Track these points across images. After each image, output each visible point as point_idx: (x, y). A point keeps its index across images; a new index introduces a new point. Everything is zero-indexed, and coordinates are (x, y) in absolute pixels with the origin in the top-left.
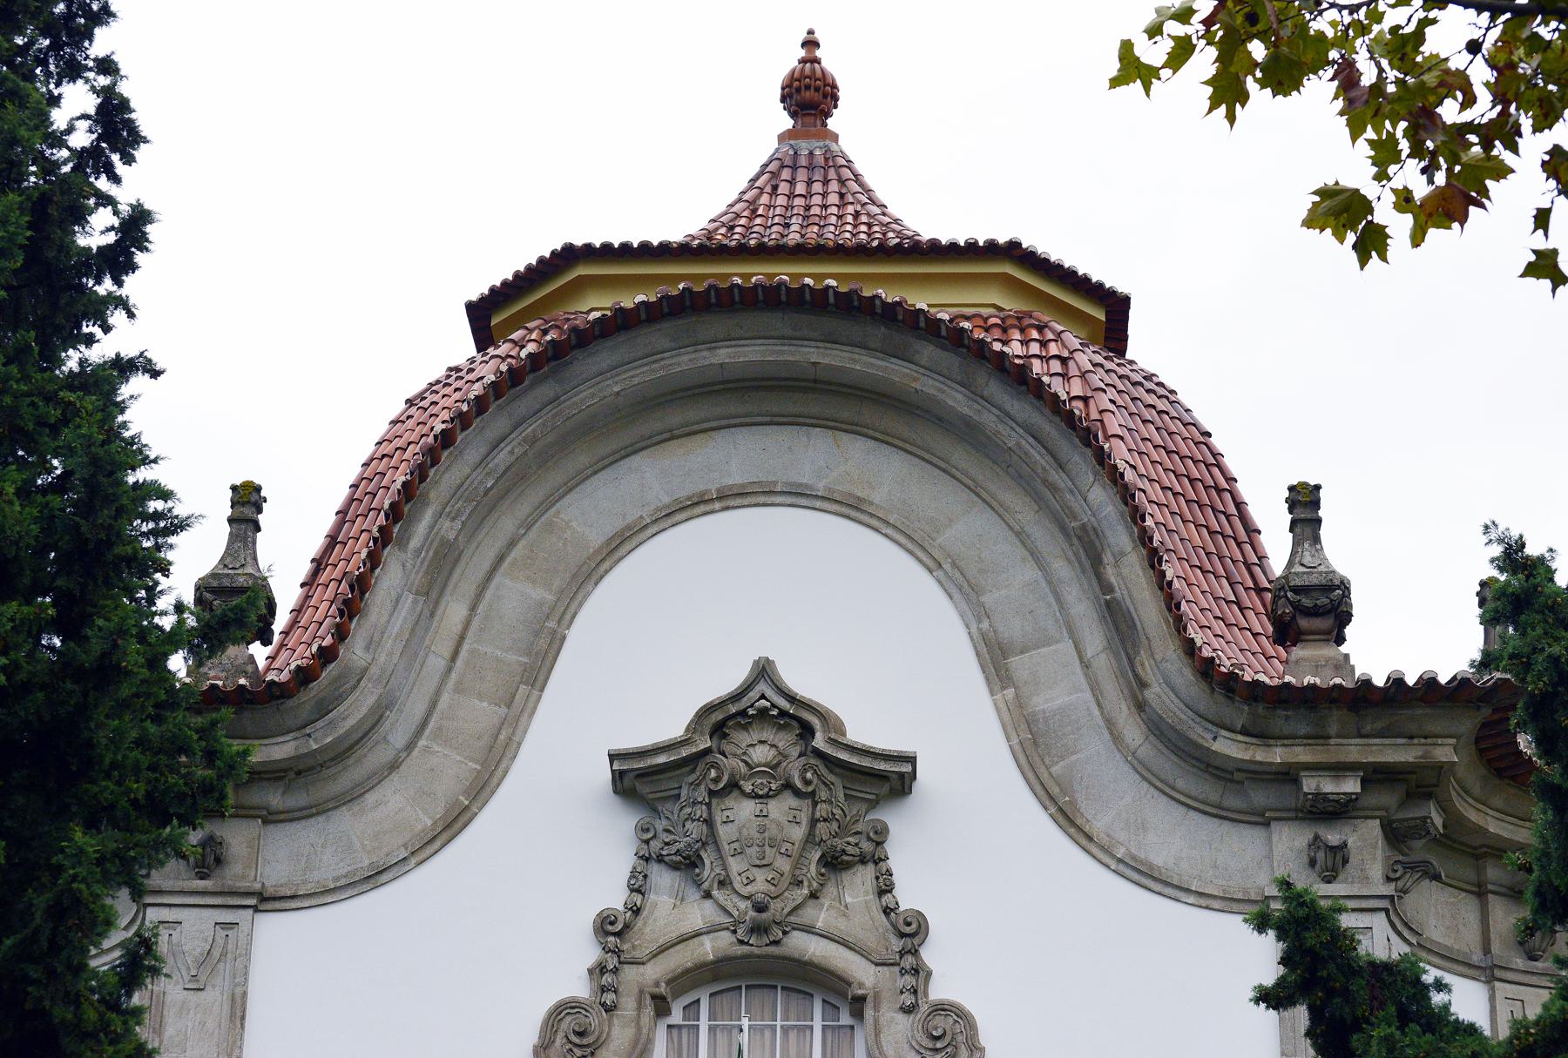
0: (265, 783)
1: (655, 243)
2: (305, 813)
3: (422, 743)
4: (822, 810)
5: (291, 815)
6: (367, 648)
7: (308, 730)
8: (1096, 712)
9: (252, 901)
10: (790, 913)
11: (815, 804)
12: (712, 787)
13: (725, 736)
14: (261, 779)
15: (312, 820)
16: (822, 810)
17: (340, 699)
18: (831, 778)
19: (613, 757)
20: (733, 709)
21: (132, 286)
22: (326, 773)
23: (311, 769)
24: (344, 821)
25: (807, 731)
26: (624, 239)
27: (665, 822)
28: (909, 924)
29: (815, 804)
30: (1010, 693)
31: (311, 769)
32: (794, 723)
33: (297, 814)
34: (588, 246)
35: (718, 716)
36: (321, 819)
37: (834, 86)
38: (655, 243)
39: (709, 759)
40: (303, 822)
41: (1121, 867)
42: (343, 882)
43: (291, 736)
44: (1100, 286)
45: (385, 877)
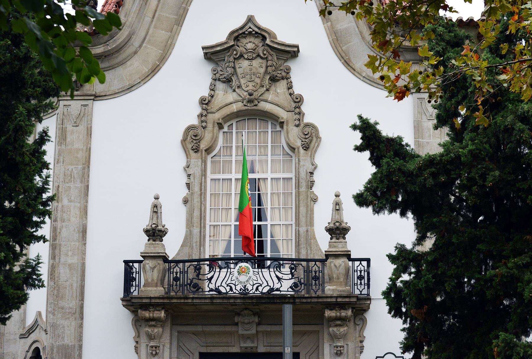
4: (270, 63)
6: (125, 16)
8: (357, 29)
11: (267, 61)
12: (235, 57)
13: (239, 40)
16: (270, 63)
18: (272, 53)
19: (203, 48)
20: (241, 32)
25: (264, 38)
27: (220, 68)
28: (297, 99)
29: (267, 61)
30: (329, 23)
32: (260, 36)
35: (236, 34)
39: (234, 48)
41: (364, 79)
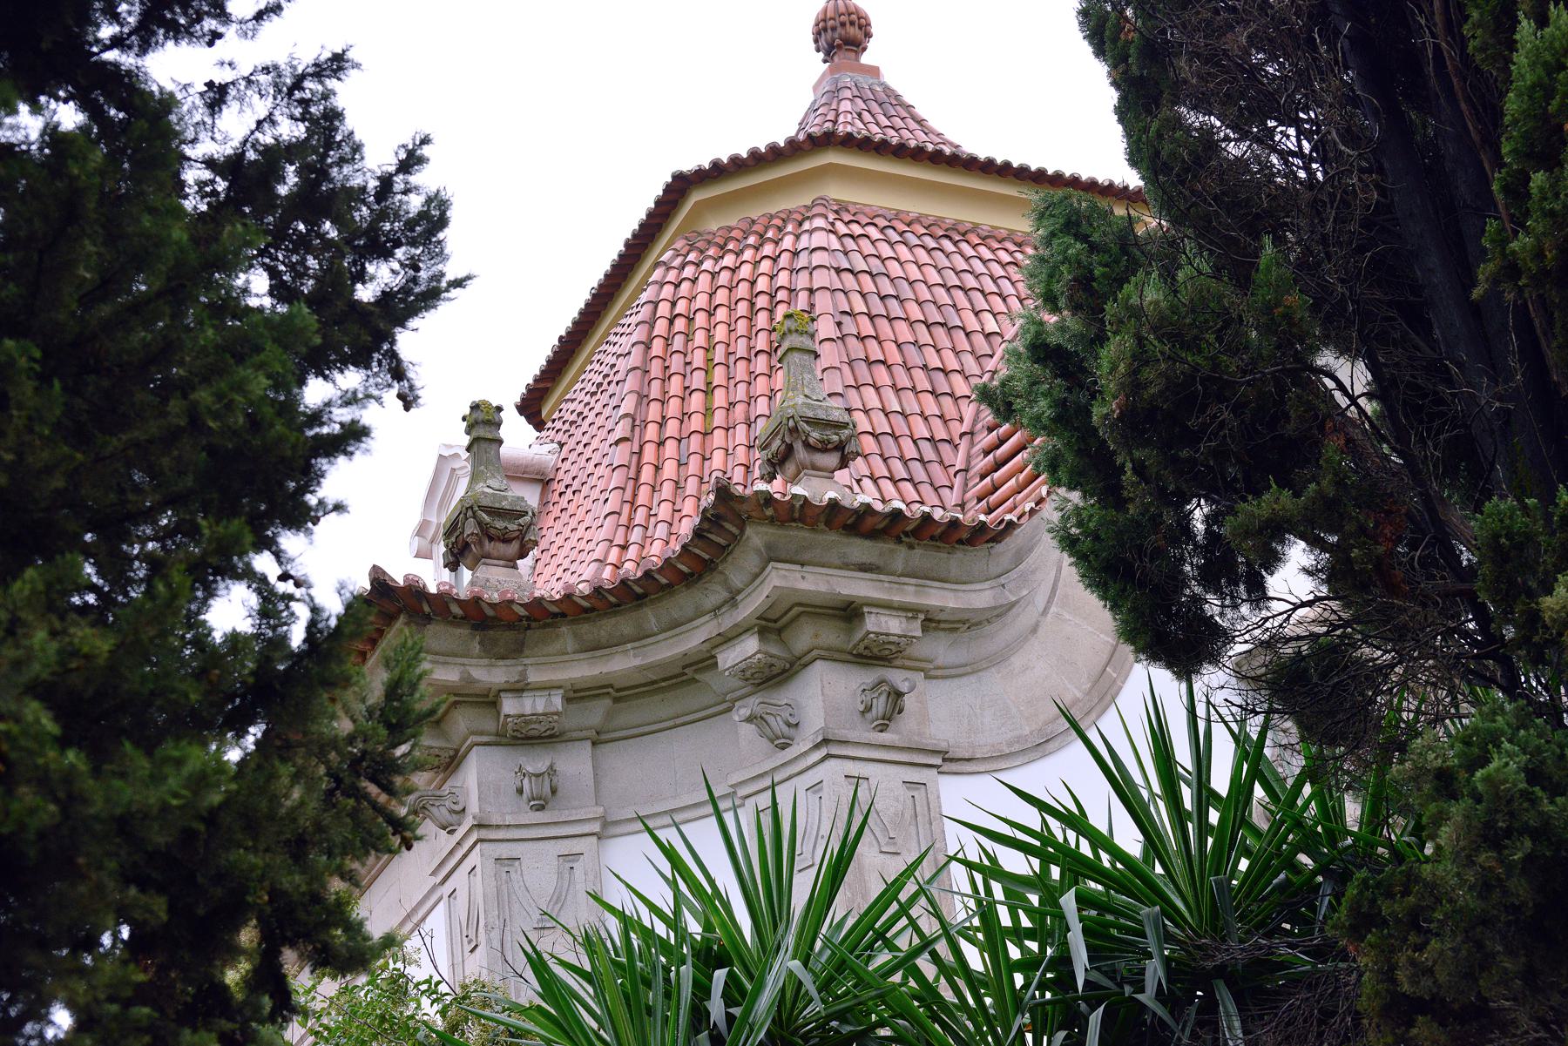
0: (942, 634)
1: (1033, 169)
2: (961, 671)
3: (1053, 609)
5: (946, 672)
7: (1002, 580)
9: (937, 761)
10: (931, 901)
14: (936, 629)
15: (965, 679)
17: (1031, 550)
21: (282, 61)
22: (988, 628)
23: (979, 623)
24: (993, 683)
26: (992, 155)
31: (979, 623)
33: (953, 672)
34: (1007, 165)
36: (973, 678)
37: (866, 18)
38: (1033, 169)
40: (948, 682)
42: (1016, 748)
43: (986, 585)
44: (659, 202)
45: (1051, 746)
